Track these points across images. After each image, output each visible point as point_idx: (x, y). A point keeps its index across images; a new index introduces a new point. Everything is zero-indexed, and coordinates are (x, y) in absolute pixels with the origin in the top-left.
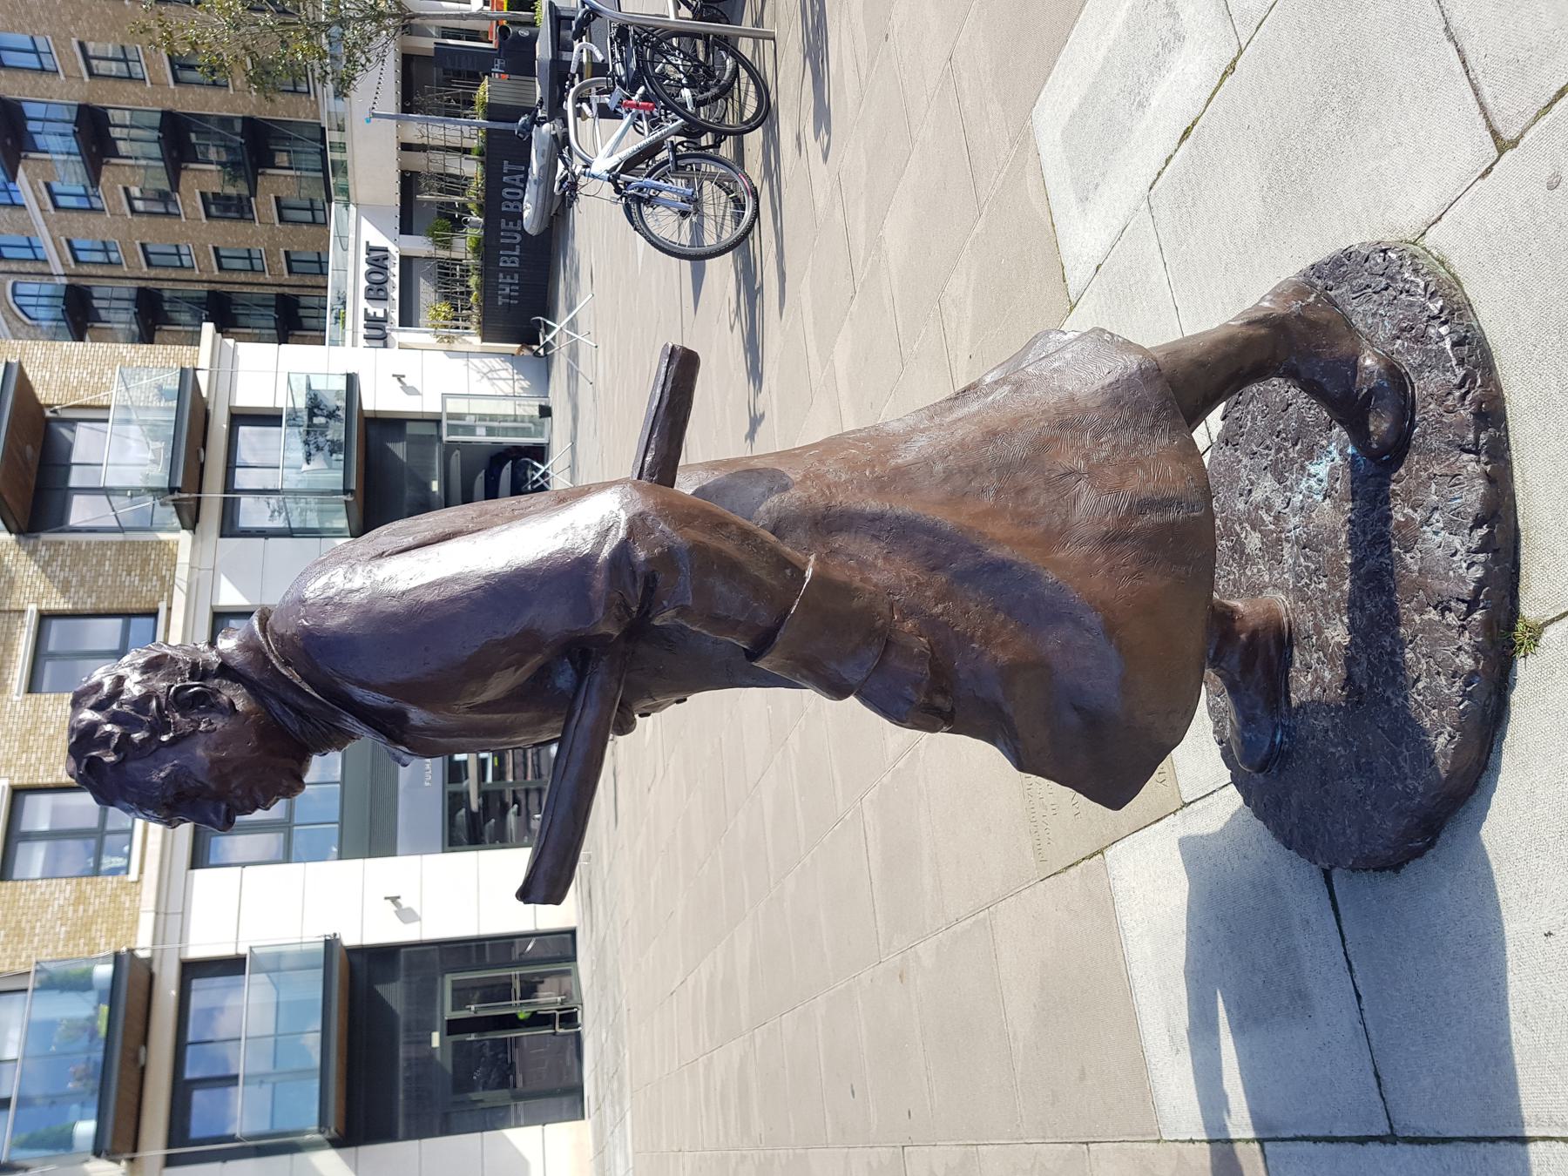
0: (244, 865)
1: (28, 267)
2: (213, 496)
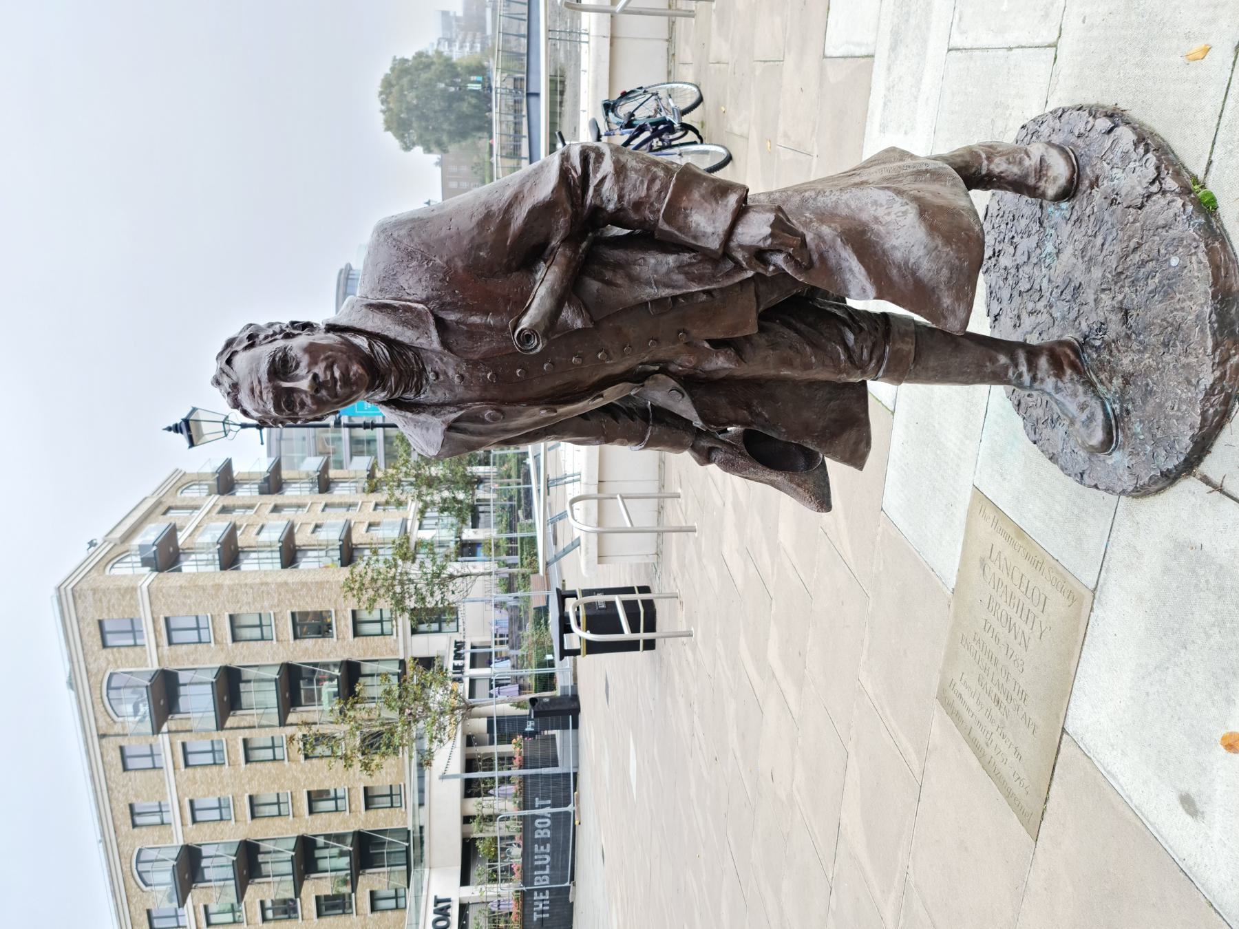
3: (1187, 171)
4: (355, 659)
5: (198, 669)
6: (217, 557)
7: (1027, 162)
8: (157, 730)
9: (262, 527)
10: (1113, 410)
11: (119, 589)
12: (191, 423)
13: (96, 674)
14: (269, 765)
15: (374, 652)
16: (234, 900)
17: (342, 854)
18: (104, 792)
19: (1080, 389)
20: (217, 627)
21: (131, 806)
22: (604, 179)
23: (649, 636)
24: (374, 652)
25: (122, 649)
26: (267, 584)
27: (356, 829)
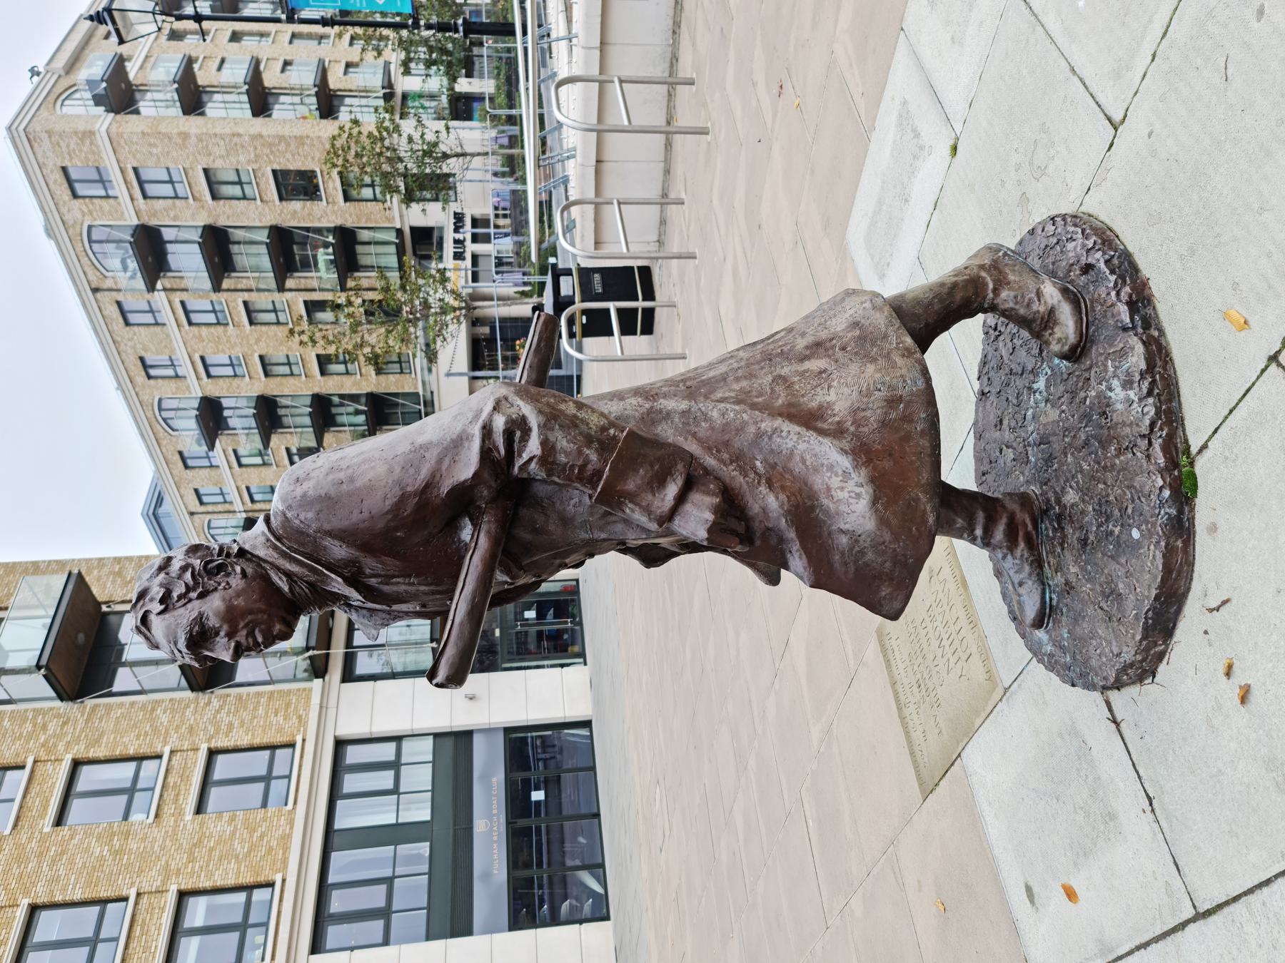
0: (352, 949)
1: (220, 508)
2: (338, 651)
3: (1184, 431)
4: (349, 224)
5: (183, 222)
6: (176, 98)
7: (1035, 307)
8: (151, 288)
9: (223, 61)
10: (1051, 599)
11: (76, 133)
12: (115, 14)
13: (73, 226)
14: (274, 328)
15: (368, 220)
16: (261, 447)
17: (357, 412)
18: (112, 348)
19: (1027, 568)
20: (192, 182)
21: (142, 359)
22: (531, 459)
23: (648, 304)
24: (368, 220)
25: (95, 201)
26: (239, 135)
27: (369, 390)
